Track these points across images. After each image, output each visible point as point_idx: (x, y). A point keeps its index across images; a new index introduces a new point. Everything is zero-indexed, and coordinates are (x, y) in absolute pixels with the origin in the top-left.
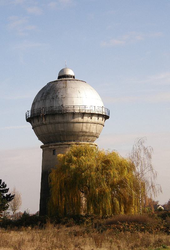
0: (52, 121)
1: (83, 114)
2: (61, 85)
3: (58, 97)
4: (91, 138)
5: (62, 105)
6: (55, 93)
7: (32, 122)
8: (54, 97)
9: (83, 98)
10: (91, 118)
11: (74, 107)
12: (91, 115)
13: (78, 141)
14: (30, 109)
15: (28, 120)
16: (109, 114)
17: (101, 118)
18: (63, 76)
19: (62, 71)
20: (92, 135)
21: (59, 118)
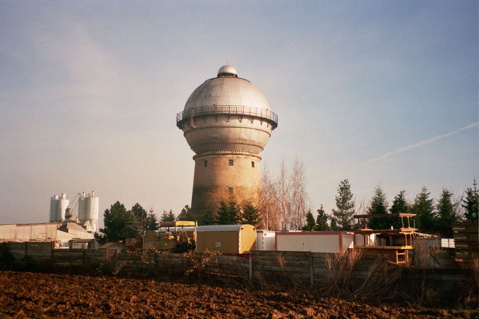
0: (203, 125)
1: (241, 116)
2: (218, 82)
3: (211, 96)
4: (252, 149)
5: (214, 105)
6: (209, 91)
7: (184, 129)
8: (206, 96)
9: (242, 98)
10: (241, 122)
11: (229, 107)
12: (252, 118)
13: (236, 151)
14: (182, 109)
15: (180, 125)
16: (277, 121)
17: (265, 124)
18: (223, 74)
19: (223, 68)
20: (253, 144)
21: (211, 121)
